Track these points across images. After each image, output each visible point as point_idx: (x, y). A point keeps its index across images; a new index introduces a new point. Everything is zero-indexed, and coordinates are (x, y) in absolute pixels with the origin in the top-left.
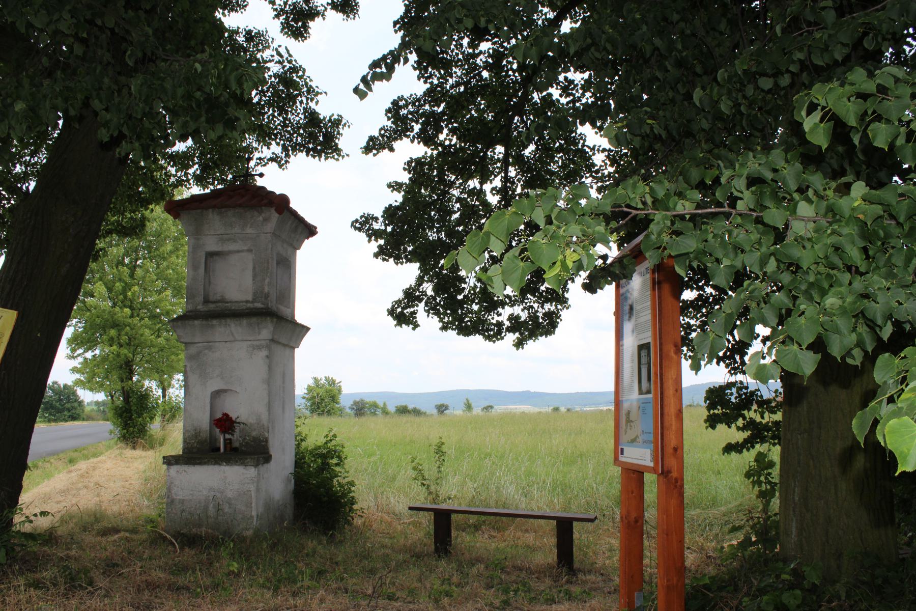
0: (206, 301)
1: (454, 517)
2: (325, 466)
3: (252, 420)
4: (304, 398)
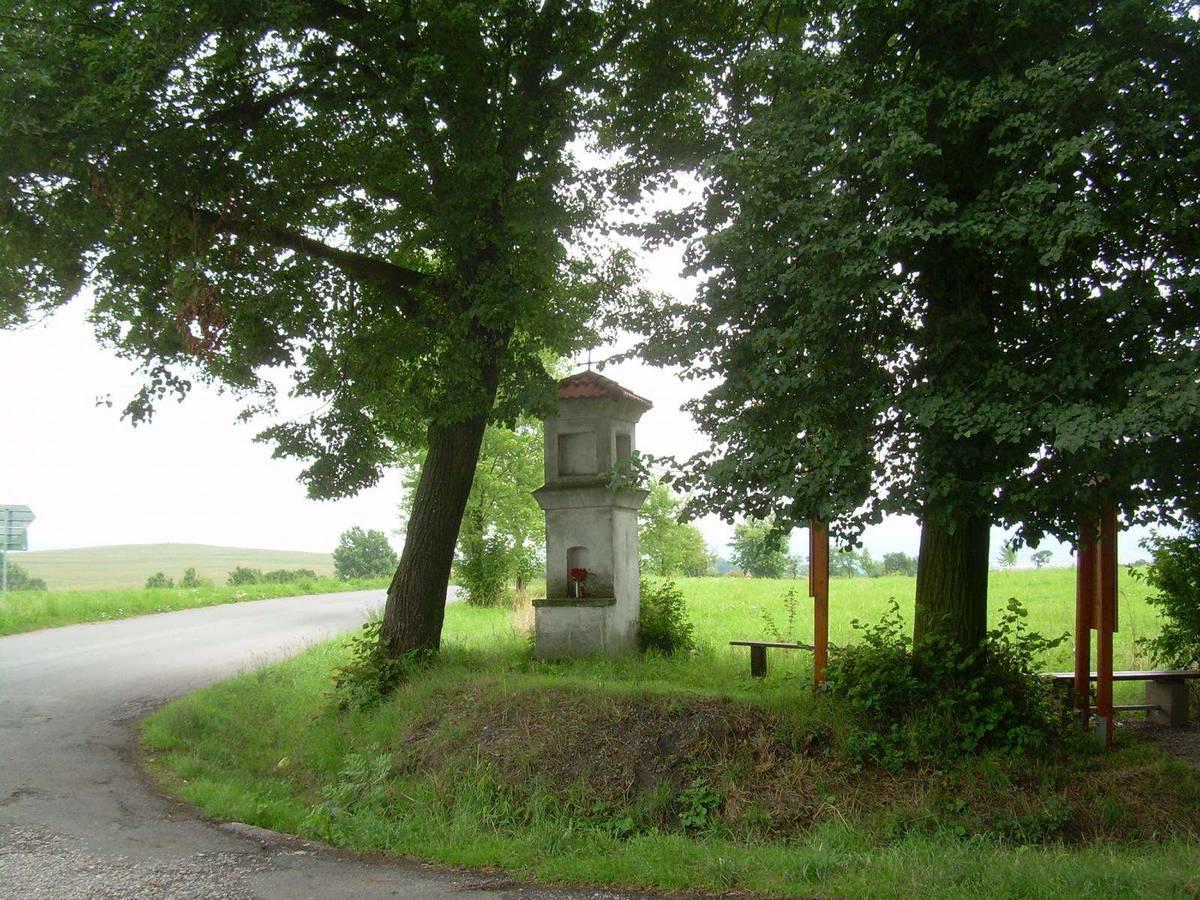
0: (561, 474)
1: (770, 651)
2: (667, 611)
3: (601, 571)
4: (730, 545)
